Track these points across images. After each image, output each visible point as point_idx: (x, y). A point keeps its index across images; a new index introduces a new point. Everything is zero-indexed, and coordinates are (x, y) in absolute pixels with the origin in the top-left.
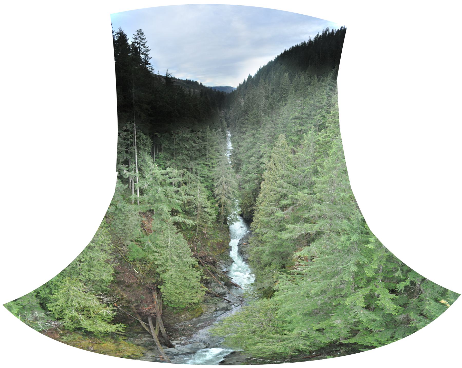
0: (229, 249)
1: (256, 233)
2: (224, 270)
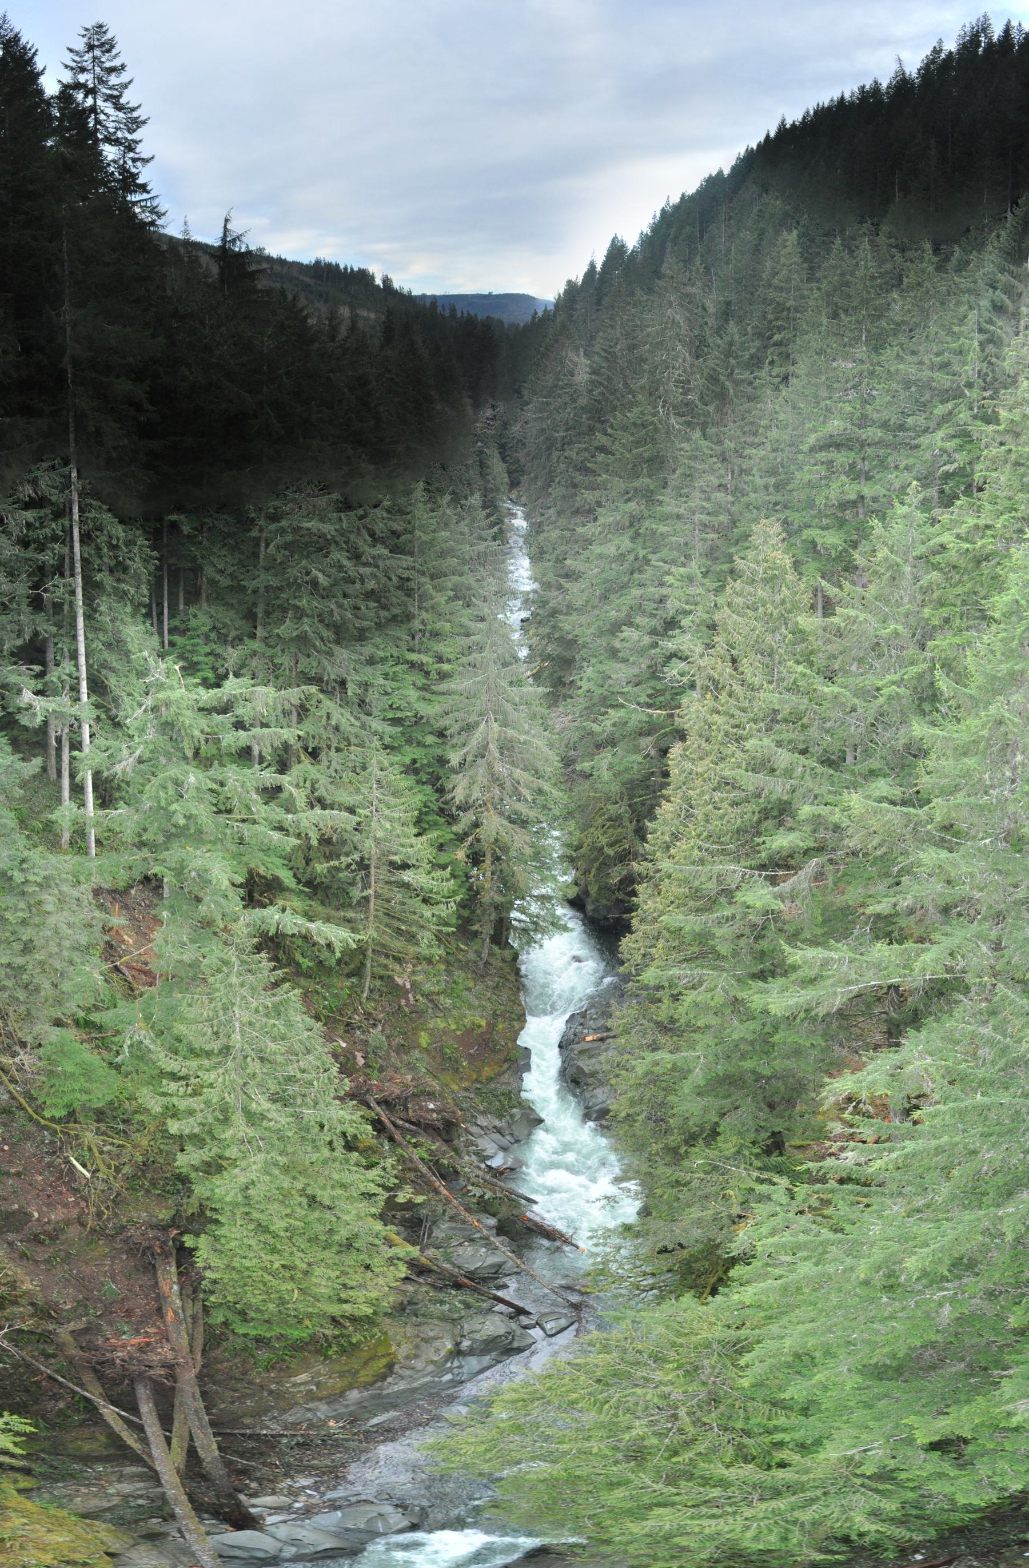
0: (519, 1061)
1: (646, 987)
2: (496, 1162)
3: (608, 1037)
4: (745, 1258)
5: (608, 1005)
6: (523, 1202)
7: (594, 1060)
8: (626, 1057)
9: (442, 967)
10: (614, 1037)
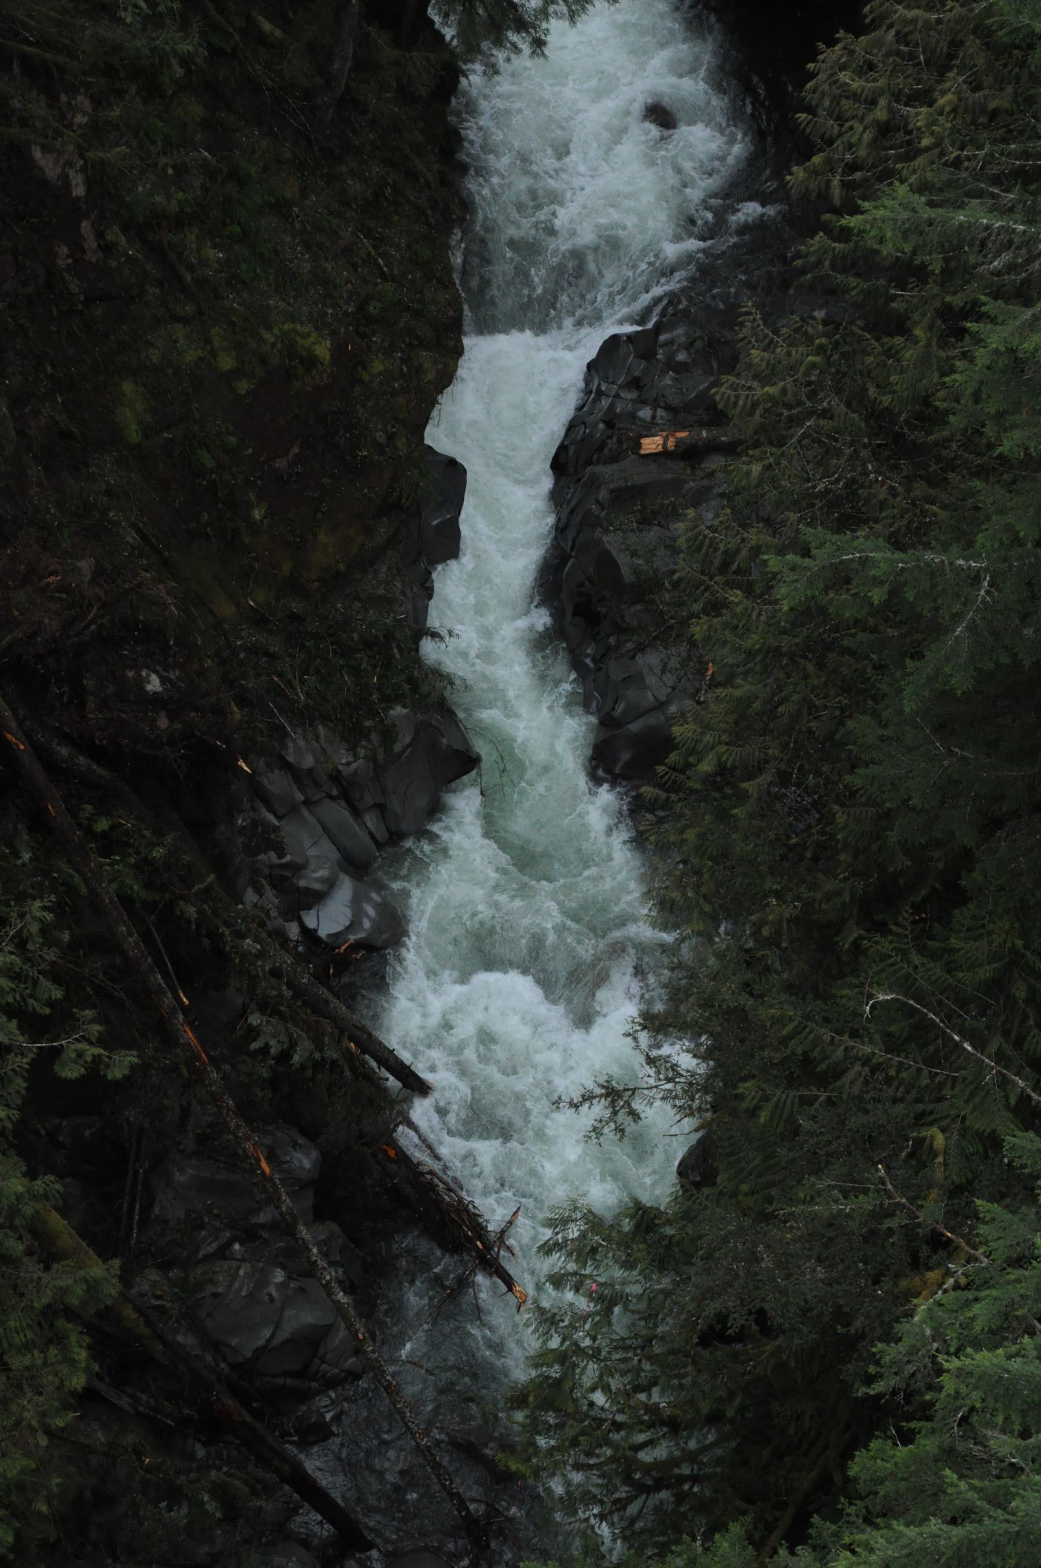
0: (425, 508)
1: (863, 262)
2: (330, 919)
3: (713, 448)
4: (900, 1413)
5: (731, 316)
6: (392, 1083)
7: (653, 534)
8: (756, 535)
9: (194, 109)
10: (731, 449)
